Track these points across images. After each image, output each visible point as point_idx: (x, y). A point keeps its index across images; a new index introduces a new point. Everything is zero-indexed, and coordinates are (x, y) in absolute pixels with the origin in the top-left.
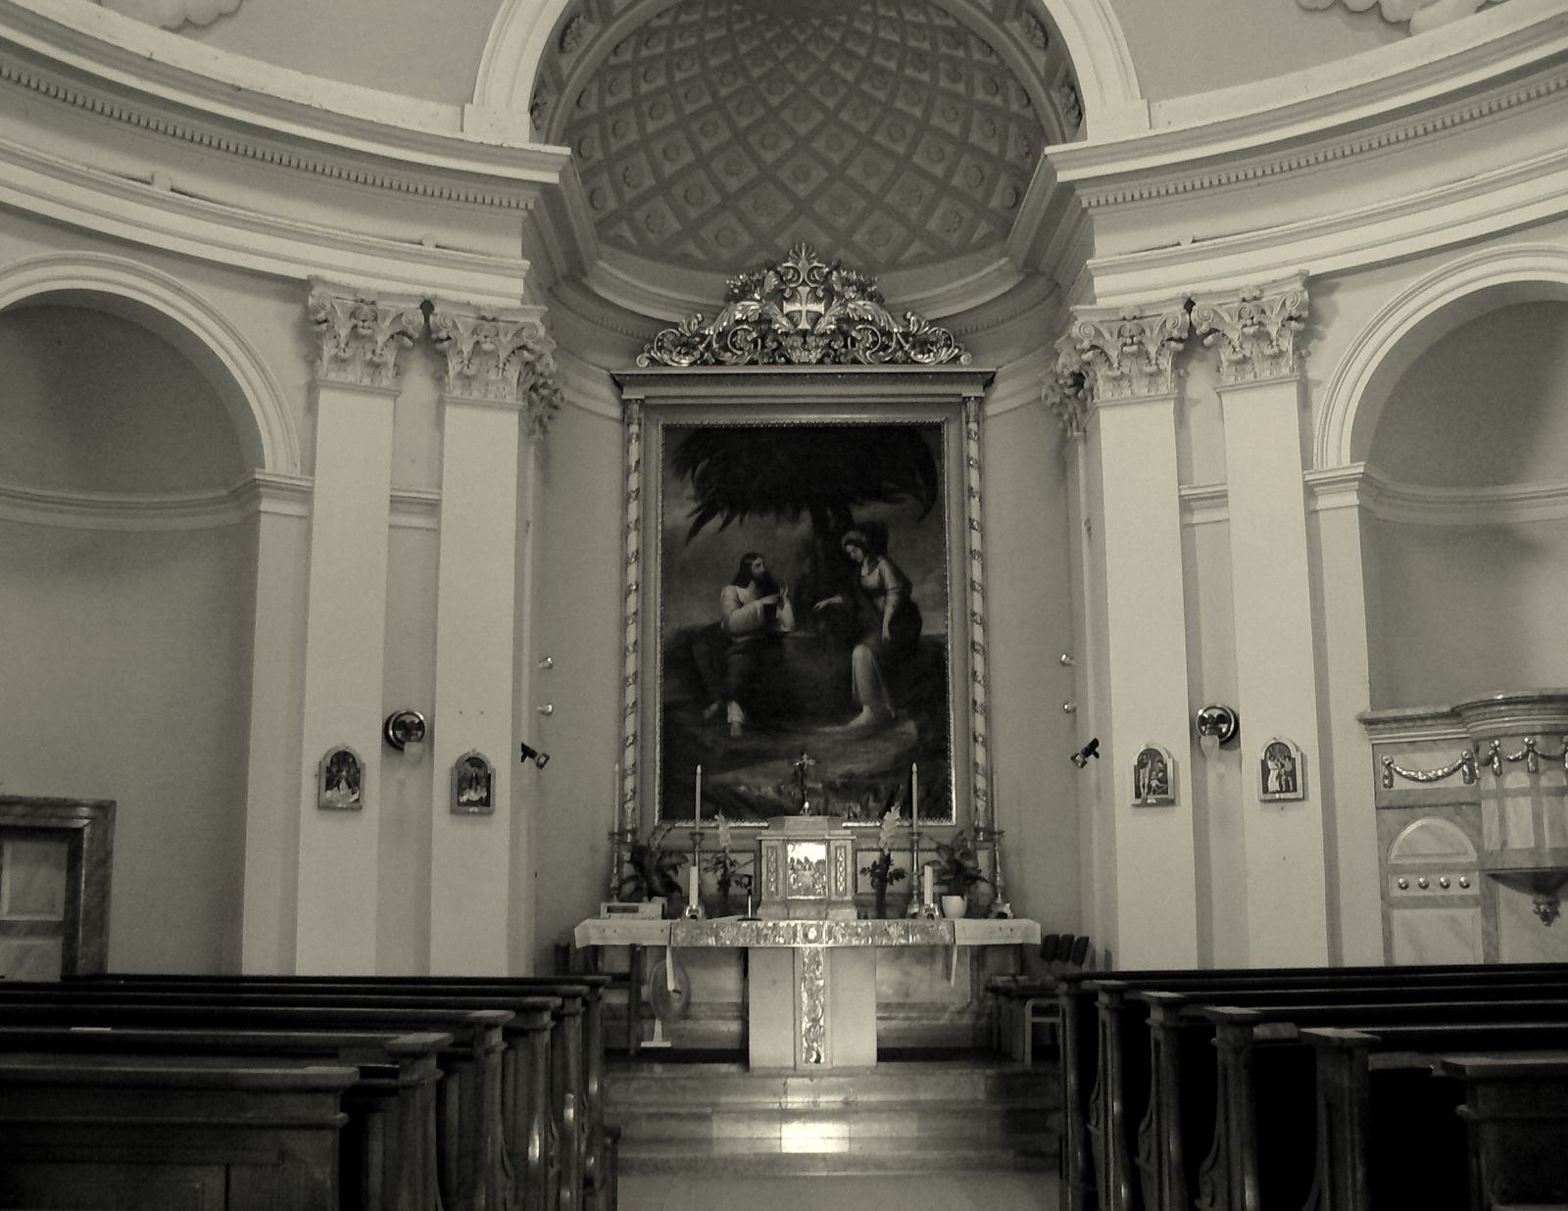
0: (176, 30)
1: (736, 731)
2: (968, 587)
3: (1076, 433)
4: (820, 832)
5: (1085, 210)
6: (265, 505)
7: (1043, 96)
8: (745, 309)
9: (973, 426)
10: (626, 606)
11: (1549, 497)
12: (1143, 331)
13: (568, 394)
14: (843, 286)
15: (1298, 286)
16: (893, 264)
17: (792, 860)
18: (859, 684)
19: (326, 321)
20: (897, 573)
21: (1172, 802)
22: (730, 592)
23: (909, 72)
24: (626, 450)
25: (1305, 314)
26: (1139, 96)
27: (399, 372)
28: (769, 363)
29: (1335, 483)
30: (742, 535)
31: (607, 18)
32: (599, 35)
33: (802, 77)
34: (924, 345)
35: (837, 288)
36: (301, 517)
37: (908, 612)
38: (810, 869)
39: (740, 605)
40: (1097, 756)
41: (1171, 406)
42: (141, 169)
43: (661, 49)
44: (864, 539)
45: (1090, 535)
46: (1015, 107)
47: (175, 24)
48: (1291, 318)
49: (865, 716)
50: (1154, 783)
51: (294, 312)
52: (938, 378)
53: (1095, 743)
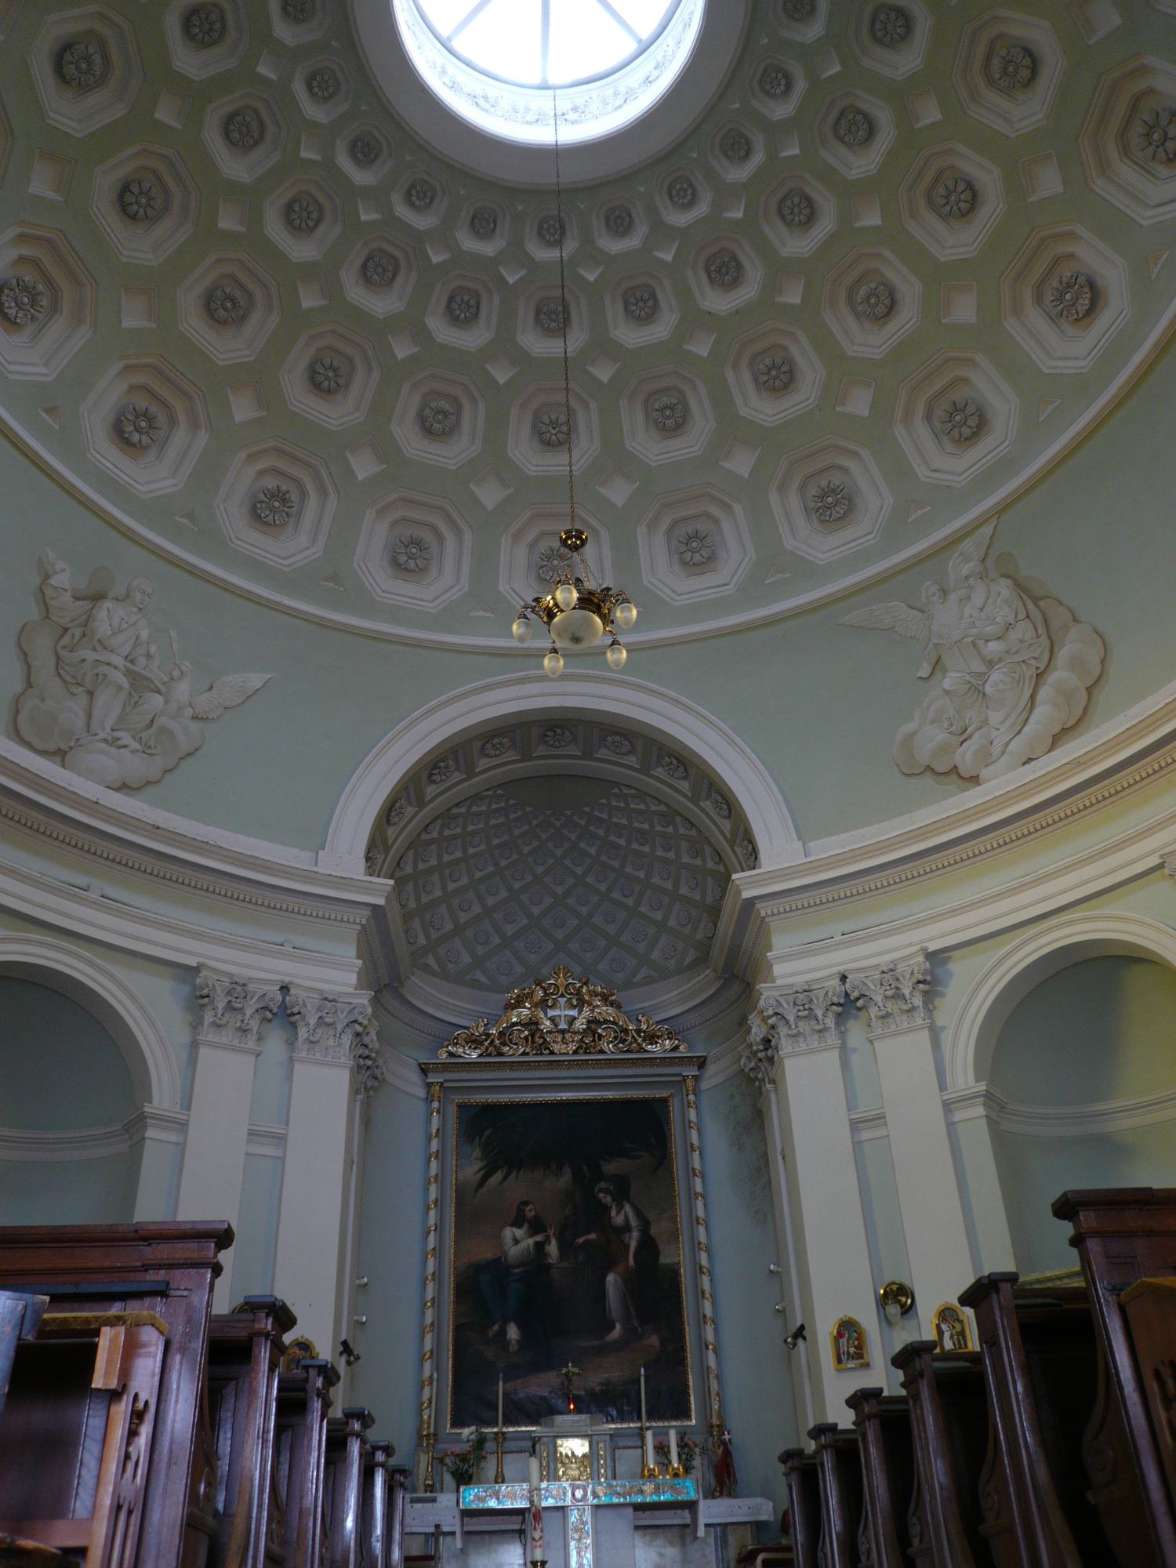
0: (116, 790)
1: (514, 1348)
2: (695, 1222)
3: (768, 1086)
4: (584, 1429)
5: (764, 918)
6: (150, 1133)
7: (730, 851)
8: (518, 1016)
9: (692, 1097)
10: (429, 1168)
11: (1131, 1109)
12: (812, 1000)
13: (389, 1077)
14: (591, 996)
15: (921, 959)
16: (628, 985)
17: (561, 1453)
18: (611, 1303)
19: (208, 996)
20: (639, 1214)
21: (867, 1365)
22: (509, 1232)
23: (635, 846)
24: (429, 1121)
25: (929, 978)
26: (796, 839)
27: (260, 1039)
28: (536, 1054)
29: (967, 1099)
30: (517, 1187)
31: (421, 804)
32: (414, 816)
33: (559, 852)
34: (652, 1038)
35: (586, 998)
36: (178, 1144)
37: (648, 1245)
38: (576, 1462)
39: (516, 1242)
40: (804, 1338)
41: (836, 1054)
42: (81, 881)
43: (458, 830)
44: (612, 1188)
45: (784, 1162)
46: (710, 865)
47: (118, 785)
48: (919, 982)
49: (617, 1332)
50: (852, 1350)
51: (186, 989)
52: (663, 1061)
53: (802, 1327)
